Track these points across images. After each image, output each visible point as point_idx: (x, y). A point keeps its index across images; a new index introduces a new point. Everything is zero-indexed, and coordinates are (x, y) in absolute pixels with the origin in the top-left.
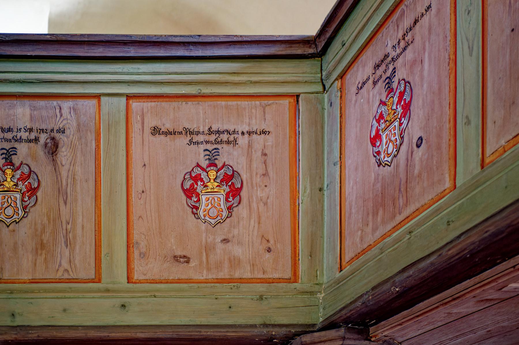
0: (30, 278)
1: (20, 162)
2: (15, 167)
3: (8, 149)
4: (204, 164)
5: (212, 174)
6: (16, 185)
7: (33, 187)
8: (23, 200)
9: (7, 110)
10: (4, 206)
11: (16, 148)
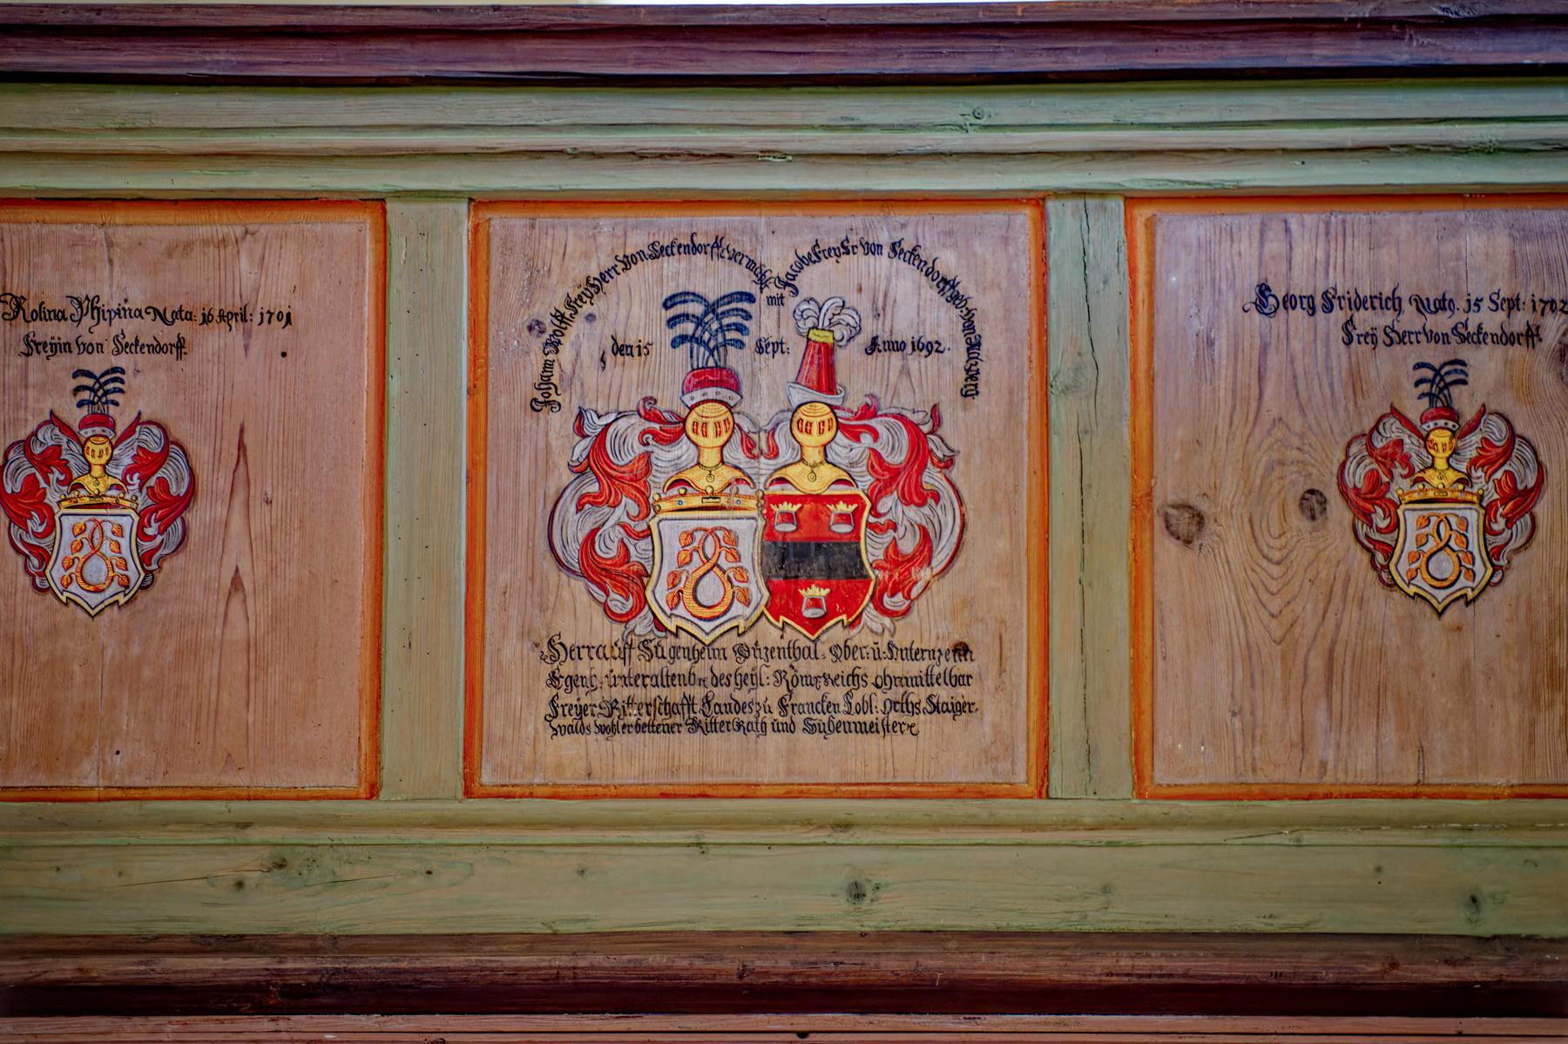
0: (1515, 782)
1: (1477, 407)
2: (1463, 422)
3: (1437, 366)
4: (74, 415)
5: (97, 449)
6: (1466, 481)
7: (1520, 487)
8: (1487, 530)
9: (1435, 241)
10: (1425, 548)
11: (1464, 364)
